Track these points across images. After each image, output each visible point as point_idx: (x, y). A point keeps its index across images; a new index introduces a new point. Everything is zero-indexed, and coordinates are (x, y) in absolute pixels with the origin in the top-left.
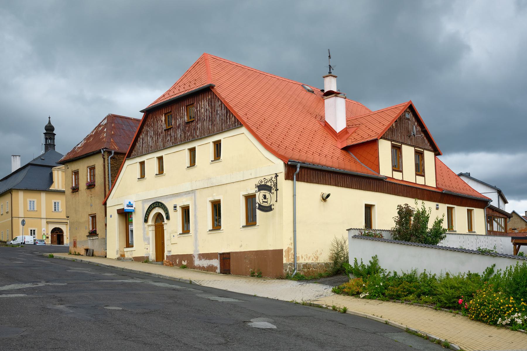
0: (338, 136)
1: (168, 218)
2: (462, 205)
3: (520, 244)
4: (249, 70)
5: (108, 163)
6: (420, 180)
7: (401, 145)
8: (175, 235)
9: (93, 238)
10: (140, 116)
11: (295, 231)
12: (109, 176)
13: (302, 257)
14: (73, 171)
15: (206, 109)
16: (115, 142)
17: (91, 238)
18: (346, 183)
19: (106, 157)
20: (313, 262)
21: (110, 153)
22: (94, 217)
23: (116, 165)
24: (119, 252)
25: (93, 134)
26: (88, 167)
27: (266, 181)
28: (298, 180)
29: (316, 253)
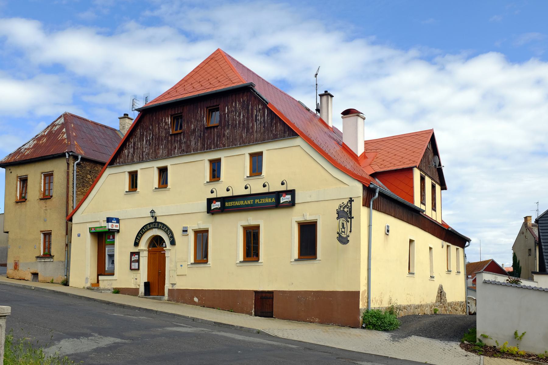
1: (173, 243)
5: (74, 170)
8: (185, 265)
9: (46, 260)
12: (73, 186)
14: (19, 177)
15: (259, 108)
17: (43, 260)
19: (71, 162)
21: (76, 158)
22: (47, 235)
23: (81, 173)
25: (46, 134)
26: (42, 173)
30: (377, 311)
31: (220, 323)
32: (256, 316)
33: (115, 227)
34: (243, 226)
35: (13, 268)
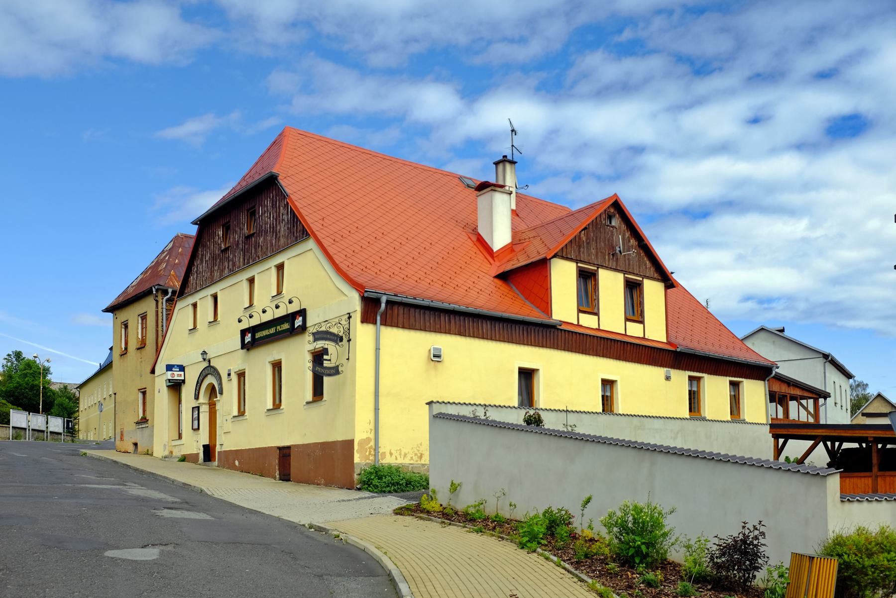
0: (496, 257)
1: (221, 393)
2: (698, 370)
3: (787, 438)
4: (384, 159)
6: (635, 330)
7: (596, 268)
10: (193, 230)
11: (377, 409)
13: (391, 454)
14: (123, 322)
15: (285, 204)
16: (177, 276)
17: (140, 426)
18: (480, 331)
19: (160, 298)
20: (412, 462)
24: (167, 446)
26: (139, 315)
27: (328, 325)
28: (385, 323)
29: (419, 447)
30: (864, 532)
31: (150, 473)
32: (280, 480)
33: (178, 376)
34: (272, 363)
35: (120, 439)
